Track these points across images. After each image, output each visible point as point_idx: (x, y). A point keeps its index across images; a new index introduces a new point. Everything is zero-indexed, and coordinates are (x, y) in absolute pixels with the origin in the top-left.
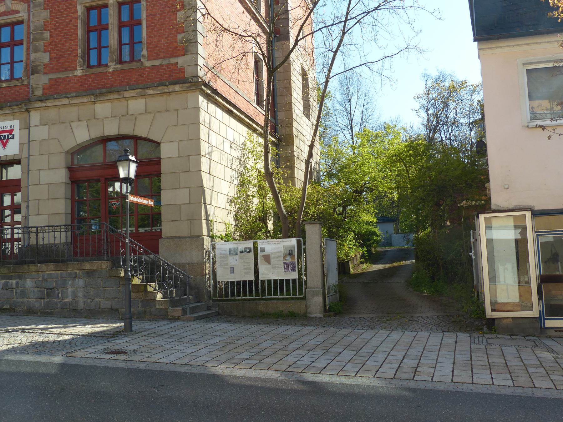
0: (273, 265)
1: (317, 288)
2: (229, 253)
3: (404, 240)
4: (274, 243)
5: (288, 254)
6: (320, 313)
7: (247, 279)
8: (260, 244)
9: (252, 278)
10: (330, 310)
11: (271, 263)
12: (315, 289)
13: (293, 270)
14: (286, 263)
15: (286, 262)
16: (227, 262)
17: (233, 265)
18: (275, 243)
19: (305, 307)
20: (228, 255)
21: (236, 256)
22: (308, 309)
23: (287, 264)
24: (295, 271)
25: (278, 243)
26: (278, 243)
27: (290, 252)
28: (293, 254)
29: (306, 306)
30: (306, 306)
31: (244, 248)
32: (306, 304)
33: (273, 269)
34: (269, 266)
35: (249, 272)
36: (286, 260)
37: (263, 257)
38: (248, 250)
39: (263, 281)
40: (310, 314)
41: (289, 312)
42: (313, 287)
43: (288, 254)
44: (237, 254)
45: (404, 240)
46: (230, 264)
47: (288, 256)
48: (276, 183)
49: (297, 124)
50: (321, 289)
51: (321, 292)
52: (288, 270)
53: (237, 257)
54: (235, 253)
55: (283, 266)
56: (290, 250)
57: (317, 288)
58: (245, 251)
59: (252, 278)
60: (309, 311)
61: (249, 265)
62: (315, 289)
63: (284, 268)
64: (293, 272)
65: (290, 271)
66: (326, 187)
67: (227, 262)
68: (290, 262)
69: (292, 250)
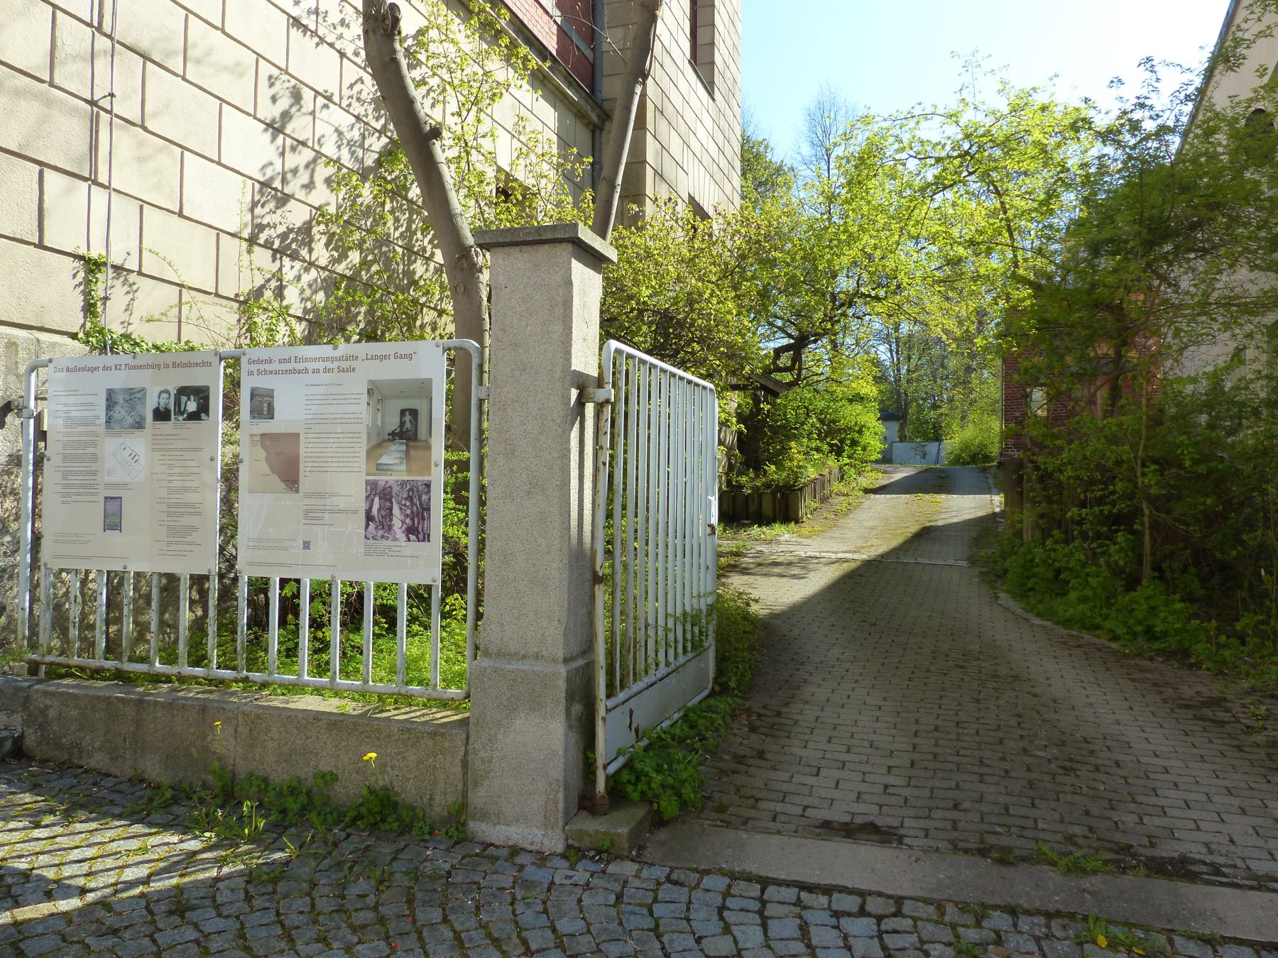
0: (309, 495)
1: (537, 656)
2: (103, 419)
3: (916, 454)
4: (321, 365)
5: (394, 436)
6: (547, 824)
7: (184, 568)
8: (251, 373)
9: (210, 565)
10: (617, 794)
11: (305, 483)
12: (525, 666)
13: (417, 531)
14: (381, 484)
15: (382, 479)
16: (94, 467)
17: (124, 486)
18: (329, 365)
19: (458, 769)
20: (101, 429)
21: (138, 433)
22: (476, 784)
23: (386, 495)
24: (427, 538)
25: (345, 365)
26: (345, 365)
27: (402, 424)
28: (422, 434)
29: (465, 763)
30: (465, 763)
31: (173, 392)
32: (466, 753)
33: (311, 516)
34: (290, 501)
35: (194, 529)
36: (380, 468)
37: (264, 446)
38: (192, 406)
39: (260, 587)
40: (484, 816)
41: (371, 791)
42: (513, 648)
43: (394, 436)
44: (139, 425)
45: (916, 454)
46: (107, 479)
47: (393, 447)
48: (565, 232)
49: (663, 125)
50: (562, 670)
51: (562, 684)
52: (390, 528)
53: (139, 443)
54: (130, 420)
55: (363, 506)
56: (403, 412)
57: (537, 656)
58: (180, 412)
59: (210, 565)
60: (479, 798)
61: (194, 490)
62: (525, 666)
63: (369, 518)
64: (415, 547)
65: (400, 535)
66: (715, 253)
67: (94, 467)
68: (403, 483)
69: (414, 413)
